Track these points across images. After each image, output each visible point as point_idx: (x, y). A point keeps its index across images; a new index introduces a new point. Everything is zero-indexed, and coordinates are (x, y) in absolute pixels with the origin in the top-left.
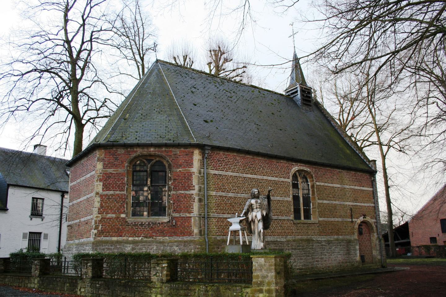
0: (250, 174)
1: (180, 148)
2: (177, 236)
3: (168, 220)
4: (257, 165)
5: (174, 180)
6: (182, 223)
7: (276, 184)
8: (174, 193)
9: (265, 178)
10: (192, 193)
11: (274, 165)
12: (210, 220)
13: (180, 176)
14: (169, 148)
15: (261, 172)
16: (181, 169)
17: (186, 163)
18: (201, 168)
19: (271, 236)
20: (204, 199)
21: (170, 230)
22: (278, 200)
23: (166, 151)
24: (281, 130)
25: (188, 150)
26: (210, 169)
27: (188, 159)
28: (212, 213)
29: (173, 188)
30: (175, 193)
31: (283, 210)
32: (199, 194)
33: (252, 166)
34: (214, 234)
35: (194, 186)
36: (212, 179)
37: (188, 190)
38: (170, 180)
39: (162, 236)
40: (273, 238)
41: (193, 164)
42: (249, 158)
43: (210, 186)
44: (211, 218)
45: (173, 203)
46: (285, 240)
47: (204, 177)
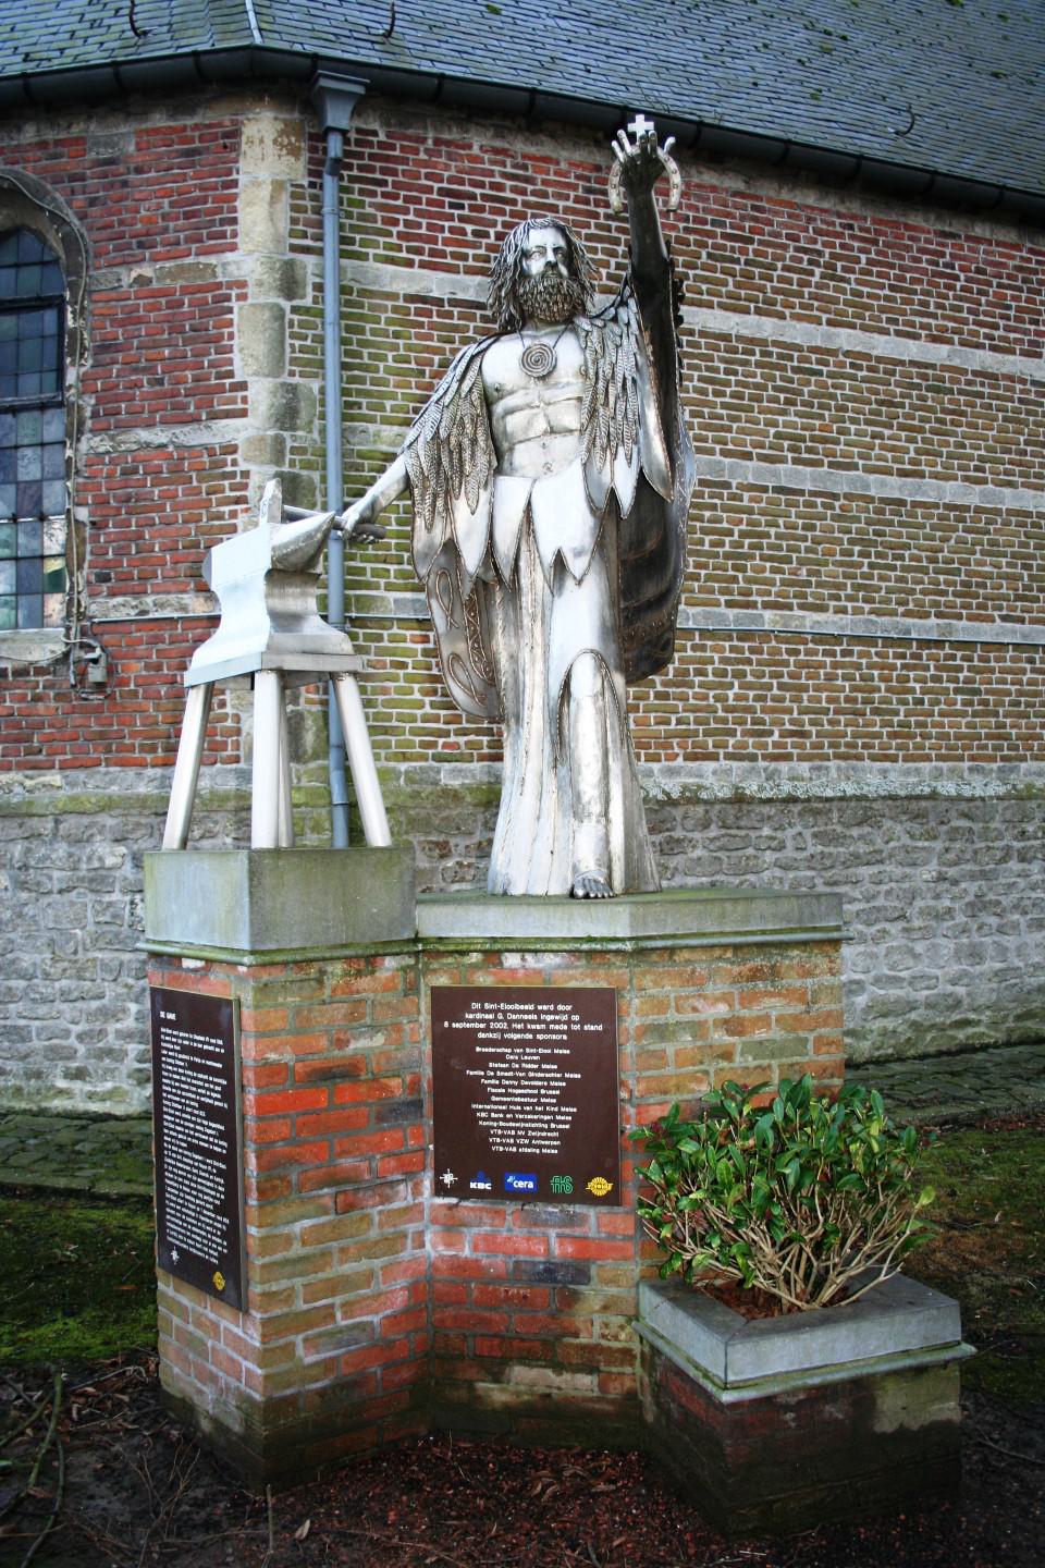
0: (723, 306)
1: (144, 114)
2: (124, 764)
3: (60, 649)
4: (784, 247)
5: (105, 347)
6: (159, 667)
7: (937, 390)
8: (102, 444)
9: (846, 339)
10: (227, 438)
11: (923, 251)
12: (379, 638)
13: (139, 321)
14: (64, 123)
15: (813, 297)
16: (147, 270)
17: (188, 215)
18: (294, 249)
19: (894, 759)
20: (324, 479)
21: (77, 719)
22: (949, 507)
23: (43, 145)
24: (996, 75)
25: (197, 120)
26: (378, 258)
27: (202, 188)
28: (389, 587)
29: (95, 414)
30: (105, 446)
31: (989, 576)
32: (279, 442)
33: (744, 251)
34: (411, 745)
35: (243, 386)
36: (397, 335)
37: (196, 420)
38: (72, 354)
39: (21, 766)
40: (907, 773)
41: (234, 221)
42: (714, 189)
43: (374, 382)
44: (383, 623)
45: (93, 523)
46: (996, 788)
47: (321, 314)
